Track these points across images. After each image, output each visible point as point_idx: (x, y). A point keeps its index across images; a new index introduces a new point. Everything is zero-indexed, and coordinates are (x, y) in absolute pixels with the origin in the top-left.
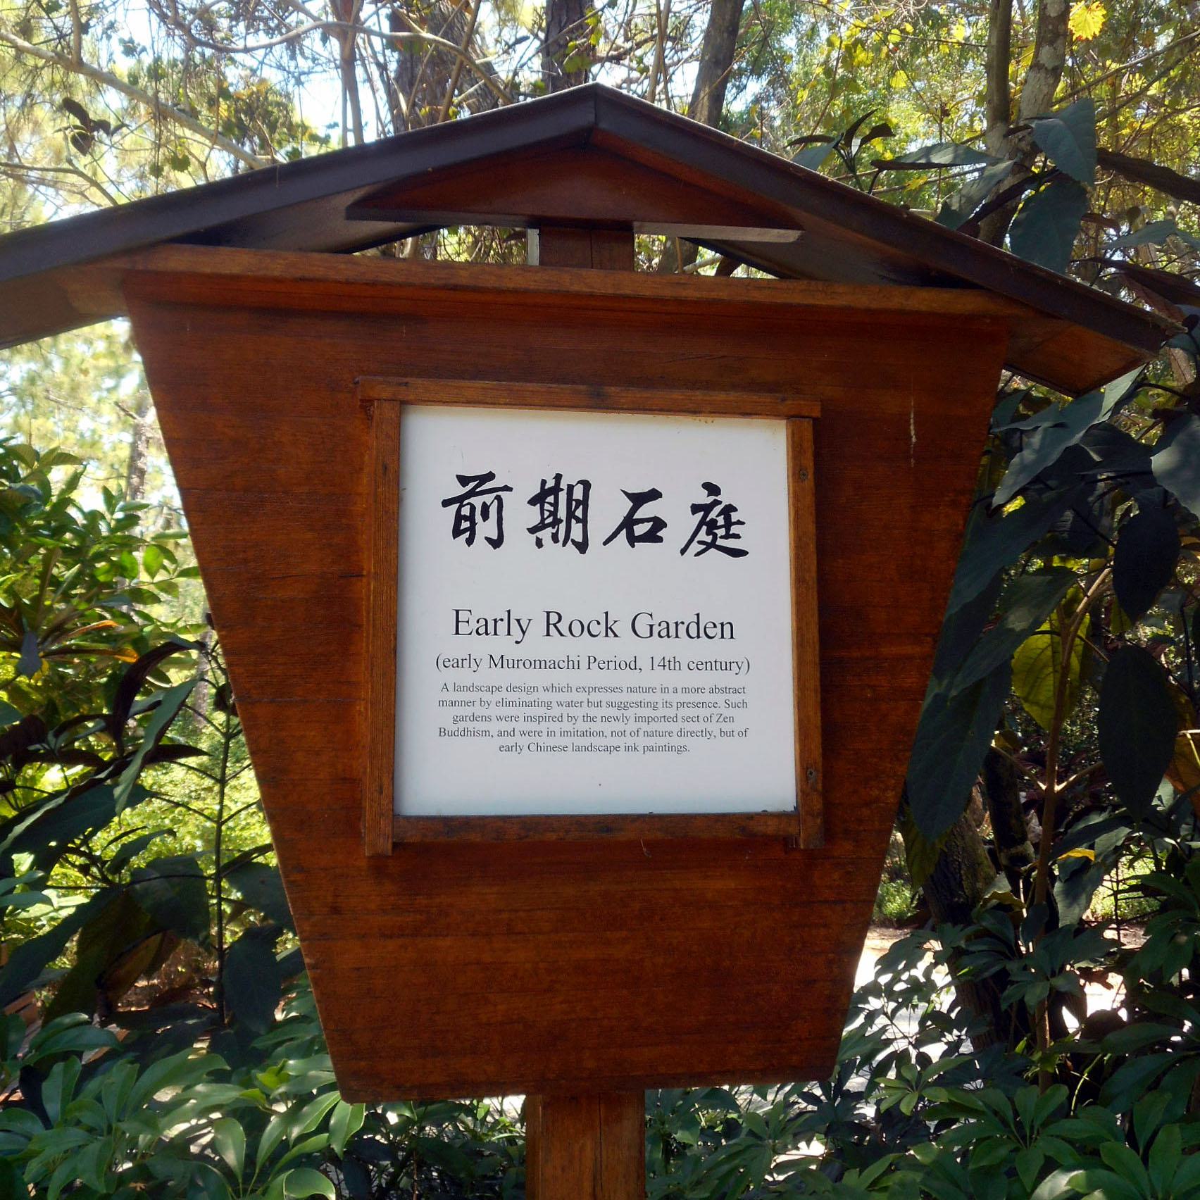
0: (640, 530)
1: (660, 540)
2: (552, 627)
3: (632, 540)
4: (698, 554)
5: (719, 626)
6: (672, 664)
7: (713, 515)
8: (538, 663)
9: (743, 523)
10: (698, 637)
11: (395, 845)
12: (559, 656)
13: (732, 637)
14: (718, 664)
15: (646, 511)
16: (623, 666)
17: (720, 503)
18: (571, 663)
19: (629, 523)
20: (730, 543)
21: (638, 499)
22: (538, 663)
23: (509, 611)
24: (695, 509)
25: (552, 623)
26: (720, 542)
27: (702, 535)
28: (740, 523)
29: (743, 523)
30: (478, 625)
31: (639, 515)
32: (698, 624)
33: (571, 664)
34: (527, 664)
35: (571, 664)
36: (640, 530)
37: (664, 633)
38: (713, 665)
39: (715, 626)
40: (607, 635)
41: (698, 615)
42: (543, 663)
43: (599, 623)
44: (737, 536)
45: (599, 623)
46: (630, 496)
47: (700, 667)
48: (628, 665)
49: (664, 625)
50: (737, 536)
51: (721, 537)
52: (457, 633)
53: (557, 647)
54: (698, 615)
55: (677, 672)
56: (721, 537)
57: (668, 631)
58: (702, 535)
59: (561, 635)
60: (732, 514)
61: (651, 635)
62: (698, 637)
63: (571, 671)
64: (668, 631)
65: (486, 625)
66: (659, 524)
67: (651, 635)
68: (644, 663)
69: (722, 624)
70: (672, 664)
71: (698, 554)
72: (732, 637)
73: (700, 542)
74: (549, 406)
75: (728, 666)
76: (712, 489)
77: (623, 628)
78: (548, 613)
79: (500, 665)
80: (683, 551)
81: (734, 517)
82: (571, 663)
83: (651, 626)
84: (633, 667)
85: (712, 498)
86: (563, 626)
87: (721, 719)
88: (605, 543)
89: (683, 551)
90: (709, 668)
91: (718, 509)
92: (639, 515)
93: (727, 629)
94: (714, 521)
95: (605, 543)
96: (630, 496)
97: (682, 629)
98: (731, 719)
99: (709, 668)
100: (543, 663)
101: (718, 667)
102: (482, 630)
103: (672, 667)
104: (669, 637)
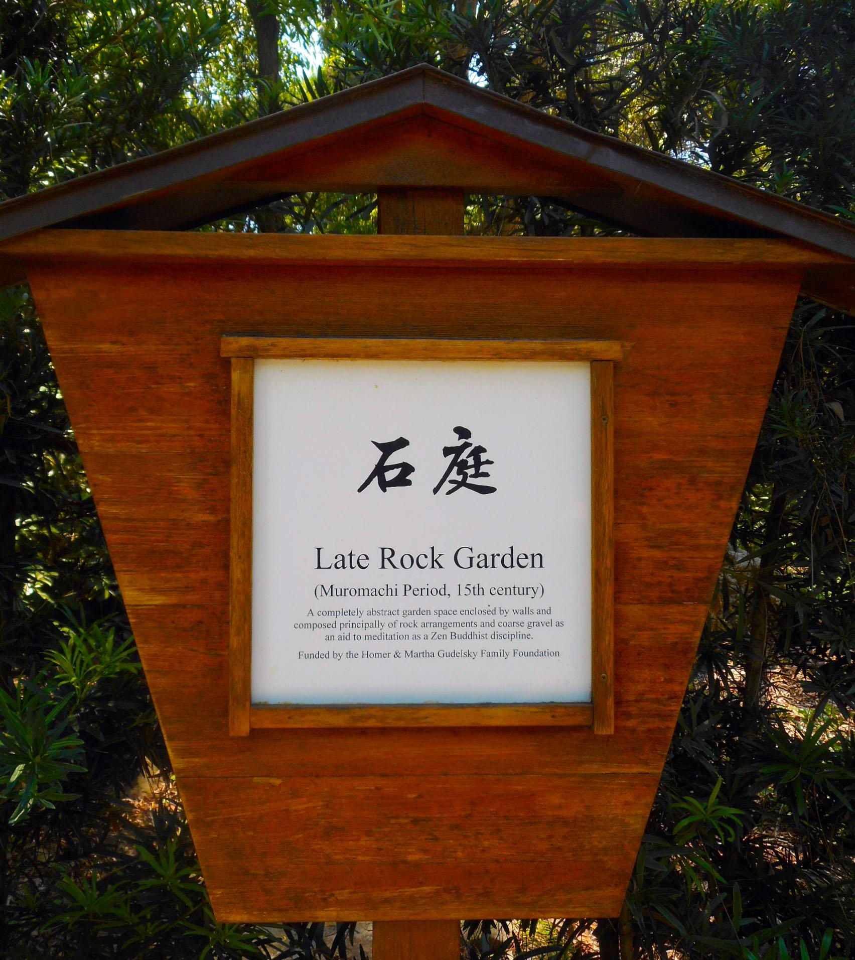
0: (390, 475)
1: (409, 483)
2: (386, 561)
3: (384, 485)
4: (449, 493)
5: (530, 557)
6: (476, 590)
7: (463, 456)
8: (361, 591)
9: (491, 463)
10: (512, 566)
12: (380, 585)
13: (541, 566)
14: (516, 590)
15: (395, 458)
16: (434, 592)
17: (470, 445)
18: (390, 591)
19: (380, 470)
20: (480, 481)
21: (387, 449)
22: (361, 591)
23: (433, 548)
24: (447, 451)
25: (387, 557)
26: (470, 481)
27: (454, 475)
28: (489, 462)
29: (491, 463)
30: (479, 560)
31: (388, 463)
32: (512, 555)
33: (390, 591)
34: (353, 592)
35: (390, 591)
36: (390, 475)
37: (482, 564)
38: (512, 591)
39: (527, 557)
40: (433, 567)
41: (512, 548)
42: (366, 591)
43: (426, 557)
44: (486, 475)
45: (426, 557)
46: (380, 446)
47: (500, 592)
49: (482, 557)
50: (486, 475)
51: (471, 476)
52: (319, 567)
53: (396, 577)
54: (512, 548)
55: (481, 596)
56: (471, 476)
57: (487, 561)
58: (454, 475)
59: (394, 567)
60: (482, 455)
61: (471, 566)
62: (512, 566)
63: (508, 596)
64: (487, 561)
65: (486, 559)
66: (407, 469)
67: (471, 566)
68: (452, 589)
69: (533, 556)
70: (476, 590)
71: (449, 493)
72: (541, 566)
73: (451, 482)
74: (523, 358)
75: (525, 591)
76: (463, 433)
77: (447, 560)
78: (383, 549)
79: (330, 594)
80: (436, 491)
81: (483, 457)
82: (390, 591)
83: (471, 559)
84: (442, 593)
85: (463, 441)
86: (396, 560)
87: (436, 636)
88: (360, 490)
89: (436, 491)
90: (508, 593)
91: (468, 451)
92: (388, 463)
93: (536, 559)
94: (465, 462)
95: (360, 490)
96: (380, 446)
97: (498, 560)
99: (508, 593)
100: (366, 591)
101: (517, 592)
102: (340, 565)
103: (476, 592)
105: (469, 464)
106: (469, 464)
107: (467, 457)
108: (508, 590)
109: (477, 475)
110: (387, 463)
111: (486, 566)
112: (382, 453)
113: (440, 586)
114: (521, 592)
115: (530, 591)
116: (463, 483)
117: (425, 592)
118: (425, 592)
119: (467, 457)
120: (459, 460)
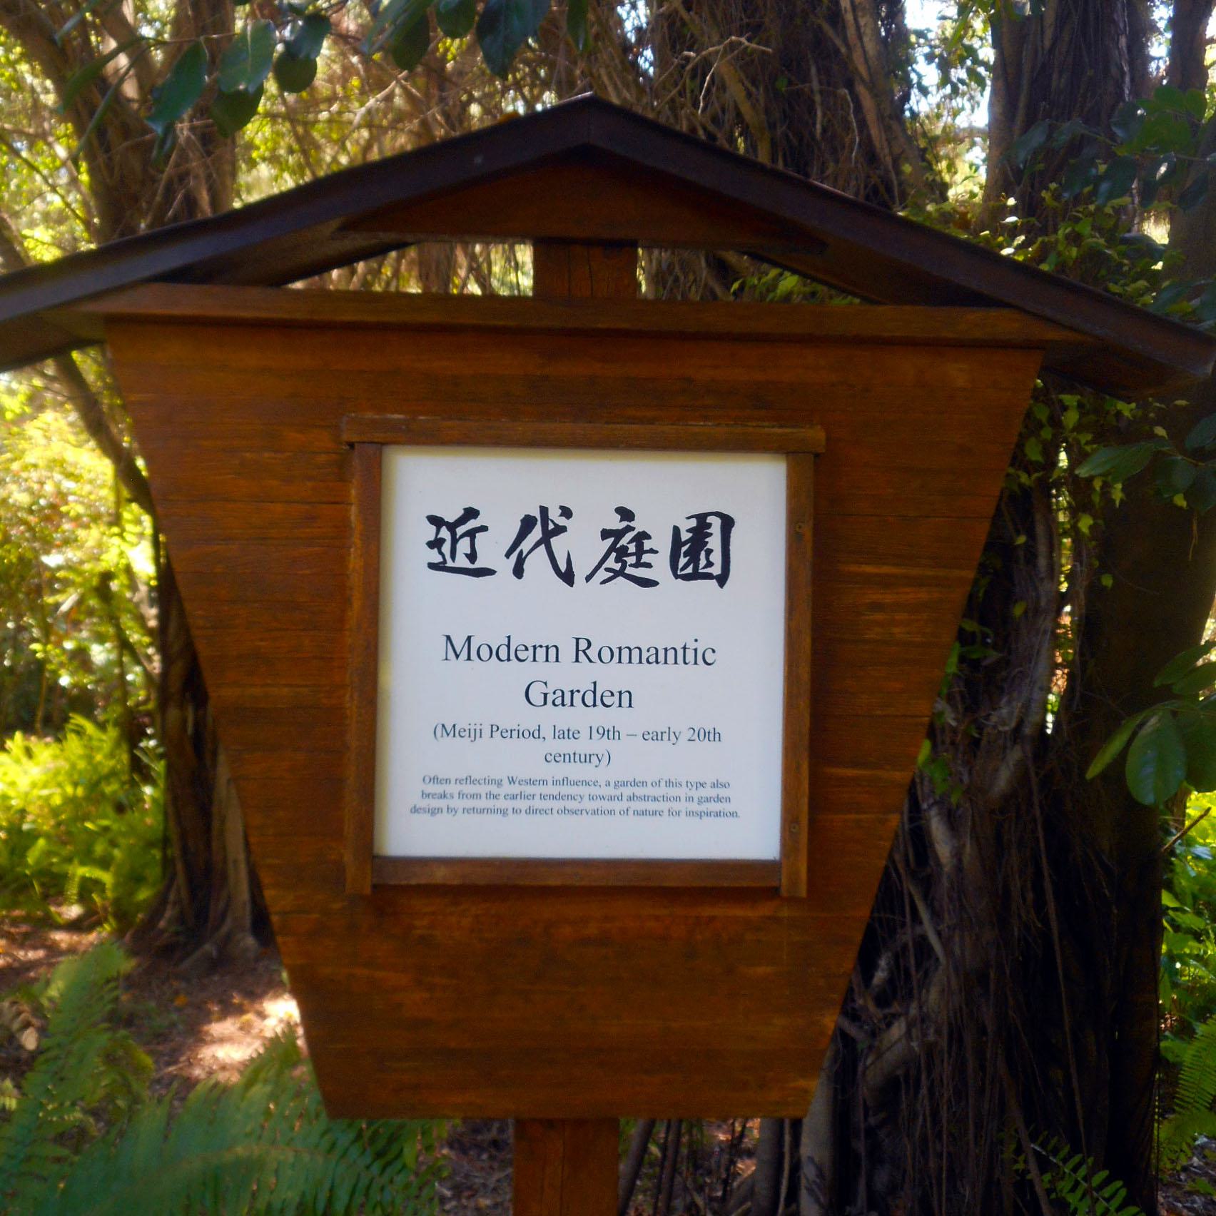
2: (581, 653)
5: (617, 695)
7: (624, 541)
9: (656, 552)
10: (594, 705)
11: (374, 887)
16: (526, 734)
17: (633, 529)
20: (641, 573)
24: (605, 534)
26: (629, 570)
28: (652, 551)
29: (656, 552)
30: (555, 696)
32: (594, 692)
37: (558, 701)
39: (612, 695)
42: (635, 653)
44: (649, 565)
47: (557, 759)
48: (531, 734)
49: (559, 693)
50: (649, 565)
51: (631, 565)
54: (595, 683)
56: (631, 565)
58: (611, 563)
59: (591, 661)
60: (645, 541)
61: (545, 703)
62: (509, 659)
65: (563, 696)
67: (545, 703)
68: (547, 732)
69: (620, 693)
72: (630, 706)
73: (608, 570)
76: (626, 514)
78: (577, 640)
81: (647, 545)
83: (545, 695)
84: (536, 735)
85: (625, 524)
86: (592, 653)
94: (625, 548)
97: (577, 697)
98: (625, 698)
100: (635, 653)
104: (563, 705)
105: (629, 552)
106: (629, 552)
107: (628, 543)
108: (567, 757)
109: (638, 564)
110: (543, 547)
111: (657, 662)
112: (477, 535)
113: (533, 728)
114: (583, 760)
115: (594, 759)
116: (621, 573)
117: (515, 734)
118: (515, 734)
119: (628, 543)
120: (618, 546)
